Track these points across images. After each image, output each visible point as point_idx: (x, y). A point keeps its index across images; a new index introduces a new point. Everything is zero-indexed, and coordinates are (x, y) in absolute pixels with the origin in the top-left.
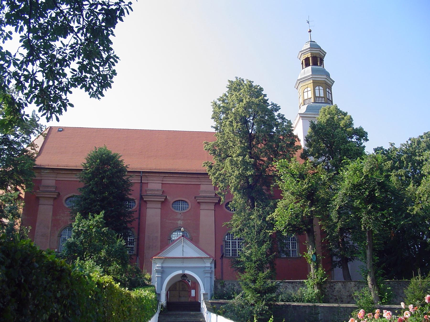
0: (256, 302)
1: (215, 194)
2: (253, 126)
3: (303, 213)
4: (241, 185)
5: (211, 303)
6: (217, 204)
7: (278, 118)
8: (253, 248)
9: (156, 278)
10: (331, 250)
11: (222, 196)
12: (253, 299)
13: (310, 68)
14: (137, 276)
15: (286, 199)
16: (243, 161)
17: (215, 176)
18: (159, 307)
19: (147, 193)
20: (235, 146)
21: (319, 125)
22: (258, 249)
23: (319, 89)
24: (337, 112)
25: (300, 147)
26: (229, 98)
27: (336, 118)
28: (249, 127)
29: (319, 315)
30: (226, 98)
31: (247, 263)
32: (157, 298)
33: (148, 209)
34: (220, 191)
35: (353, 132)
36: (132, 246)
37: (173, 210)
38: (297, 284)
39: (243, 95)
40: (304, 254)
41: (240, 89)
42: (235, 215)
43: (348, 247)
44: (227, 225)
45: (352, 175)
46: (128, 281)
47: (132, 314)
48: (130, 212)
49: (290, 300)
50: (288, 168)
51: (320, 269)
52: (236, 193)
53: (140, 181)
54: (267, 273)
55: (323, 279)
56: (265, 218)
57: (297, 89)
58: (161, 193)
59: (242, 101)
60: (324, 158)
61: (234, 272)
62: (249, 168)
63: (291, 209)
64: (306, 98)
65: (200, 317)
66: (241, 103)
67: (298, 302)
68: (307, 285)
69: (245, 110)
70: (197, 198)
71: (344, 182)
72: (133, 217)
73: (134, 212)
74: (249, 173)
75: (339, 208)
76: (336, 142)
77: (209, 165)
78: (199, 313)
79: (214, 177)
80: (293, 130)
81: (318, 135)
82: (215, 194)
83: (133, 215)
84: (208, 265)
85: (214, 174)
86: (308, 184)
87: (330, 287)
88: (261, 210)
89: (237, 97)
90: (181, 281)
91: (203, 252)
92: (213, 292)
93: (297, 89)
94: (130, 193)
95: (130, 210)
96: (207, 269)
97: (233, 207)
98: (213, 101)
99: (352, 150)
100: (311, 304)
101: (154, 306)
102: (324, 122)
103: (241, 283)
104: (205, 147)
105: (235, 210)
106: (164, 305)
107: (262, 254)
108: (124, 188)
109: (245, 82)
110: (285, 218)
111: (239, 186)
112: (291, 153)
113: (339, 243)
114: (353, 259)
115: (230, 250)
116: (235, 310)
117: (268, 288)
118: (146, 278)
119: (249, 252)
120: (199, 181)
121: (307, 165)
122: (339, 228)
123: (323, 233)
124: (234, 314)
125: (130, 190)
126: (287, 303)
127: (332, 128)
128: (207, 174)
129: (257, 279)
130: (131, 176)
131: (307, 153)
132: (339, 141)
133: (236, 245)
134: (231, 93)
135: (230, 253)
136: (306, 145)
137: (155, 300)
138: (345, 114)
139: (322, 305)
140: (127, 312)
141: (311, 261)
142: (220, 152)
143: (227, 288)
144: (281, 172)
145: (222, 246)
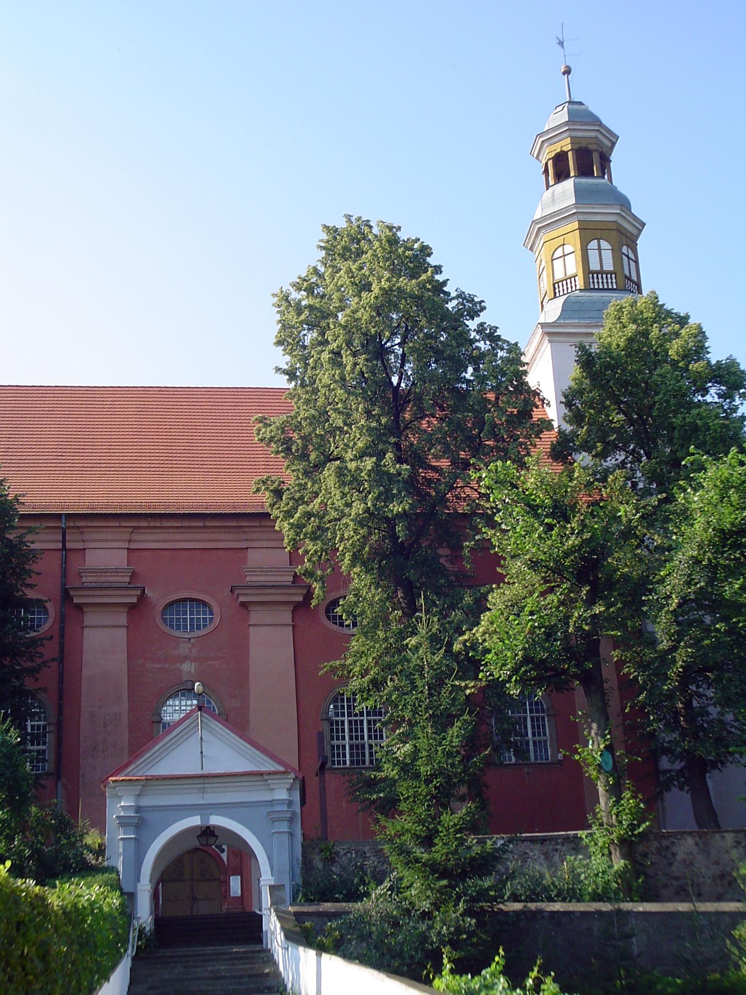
0: (436, 906)
1: (295, 576)
2: (402, 365)
3: (568, 624)
4: (371, 548)
5: (296, 914)
6: (301, 607)
7: (478, 337)
8: (420, 735)
9: (121, 843)
10: (652, 735)
11: (316, 580)
12: (428, 897)
13: (568, 185)
14: (58, 840)
15: (514, 583)
16: (378, 470)
17: (292, 521)
18: (133, 935)
19: (84, 579)
20: (350, 426)
21: (603, 356)
22: (434, 739)
23: (599, 249)
24: (657, 316)
25: (547, 424)
26: (328, 281)
27: (655, 331)
28: (391, 368)
29: (634, 940)
30: (319, 282)
31: (405, 784)
32: (127, 907)
33: (86, 631)
34: (307, 565)
35: (709, 374)
36: (41, 747)
37: (166, 629)
38: (557, 844)
39: (371, 270)
40: (576, 751)
41: (360, 253)
42: (356, 638)
43: (705, 725)
44: (333, 670)
45: (714, 501)
46: (30, 857)
47: (53, 965)
48: (33, 642)
49: (537, 896)
50: (517, 488)
51: (627, 794)
52: (357, 569)
53: (60, 546)
54: (468, 813)
55: (639, 826)
56: (450, 645)
57: (531, 249)
58: (127, 579)
59: (367, 287)
60: (621, 456)
61: (361, 814)
62: (395, 492)
63: (532, 613)
64: (559, 275)
65: (264, 962)
66: (364, 294)
67: (564, 900)
68: (587, 846)
69: (379, 315)
70: (237, 592)
71: (692, 525)
72: (41, 655)
73: (45, 642)
74: (396, 508)
75: (680, 605)
76: (657, 406)
77: (272, 488)
78: (258, 948)
79: (289, 524)
80: (525, 373)
81: (602, 387)
82: (295, 576)
83: (40, 649)
84: (282, 794)
85: (289, 514)
86: (581, 532)
87: (659, 850)
88: (436, 619)
89: (353, 277)
90: (196, 849)
91: (263, 756)
92: (299, 881)
93: (531, 249)
94: (29, 581)
95: (32, 634)
96: (277, 808)
97: (349, 613)
98: (277, 291)
99: (708, 429)
100: (606, 907)
101: (118, 934)
102: (618, 345)
103: (386, 847)
104: (257, 433)
105: (355, 624)
106: (148, 929)
107: (449, 755)
108: (12, 568)
109: (375, 231)
110: (515, 642)
111: (367, 549)
112: (521, 444)
113: (677, 713)
114: (723, 763)
115: (344, 747)
116: (370, 934)
117: (473, 859)
118: (87, 847)
119: (408, 747)
120: (244, 536)
121: (576, 475)
122: (682, 667)
123: (628, 687)
124: (369, 949)
125: (29, 573)
126: (532, 906)
127: (645, 364)
128: (268, 515)
129: (437, 832)
130: (30, 530)
131: (569, 441)
132: (668, 401)
133: (362, 730)
134: (333, 267)
135: (344, 755)
136: (565, 419)
137: (120, 913)
138: (683, 321)
139: (642, 907)
140: (36, 962)
141: (599, 772)
142: (305, 447)
143: (341, 866)
144: (494, 502)
145: (320, 735)
